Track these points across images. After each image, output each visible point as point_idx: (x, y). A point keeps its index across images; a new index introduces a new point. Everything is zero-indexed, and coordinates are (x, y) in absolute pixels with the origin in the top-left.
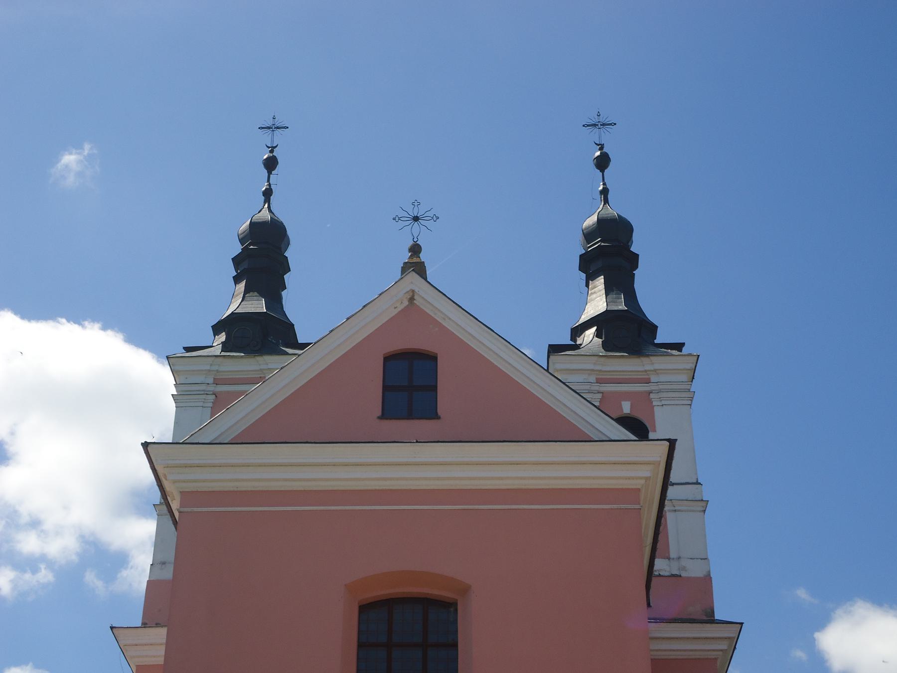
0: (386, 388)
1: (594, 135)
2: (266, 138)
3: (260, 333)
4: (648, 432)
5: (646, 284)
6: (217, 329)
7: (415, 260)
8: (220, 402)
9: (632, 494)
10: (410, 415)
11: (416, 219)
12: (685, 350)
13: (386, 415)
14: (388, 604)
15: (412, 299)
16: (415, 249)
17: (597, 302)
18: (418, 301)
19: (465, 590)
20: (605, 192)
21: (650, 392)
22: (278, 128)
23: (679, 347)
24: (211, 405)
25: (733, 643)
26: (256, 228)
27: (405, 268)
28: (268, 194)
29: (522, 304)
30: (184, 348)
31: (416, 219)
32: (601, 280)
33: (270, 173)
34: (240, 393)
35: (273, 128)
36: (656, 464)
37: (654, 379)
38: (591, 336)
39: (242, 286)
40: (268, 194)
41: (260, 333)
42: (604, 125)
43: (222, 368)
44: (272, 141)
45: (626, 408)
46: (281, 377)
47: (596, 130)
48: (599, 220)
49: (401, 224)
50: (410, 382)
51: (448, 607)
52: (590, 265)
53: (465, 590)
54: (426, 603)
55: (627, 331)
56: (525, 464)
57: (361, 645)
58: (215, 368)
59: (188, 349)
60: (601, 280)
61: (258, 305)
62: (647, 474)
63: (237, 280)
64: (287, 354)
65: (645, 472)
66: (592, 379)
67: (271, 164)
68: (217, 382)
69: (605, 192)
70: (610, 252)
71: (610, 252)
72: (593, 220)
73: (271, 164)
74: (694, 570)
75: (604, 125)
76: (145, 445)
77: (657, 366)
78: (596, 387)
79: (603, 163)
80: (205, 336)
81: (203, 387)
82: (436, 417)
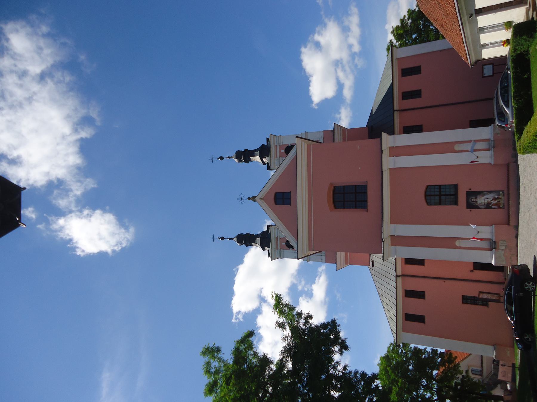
0: (283, 204)
1: (215, 160)
2: (216, 240)
3: (265, 240)
5: (251, 148)
6: (264, 250)
9: (308, 146)
13: (290, 204)
16: (249, 199)
17: (257, 158)
19: (331, 184)
20: (229, 157)
23: (268, 139)
27: (254, 201)
28: (230, 239)
29: (261, 176)
32: (251, 158)
40: (230, 239)
45: (283, 151)
50: (282, 199)
51: (335, 188)
53: (331, 184)
54: (334, 193)
56: (490, 28)
59: (269, 256)
60: (251, 158)
61: (258, 239)
67: (222, 238)
68: (277, 249)
69: (229, 157)
70: (245, 156)
71: (245, 156)
72: (236, 160)
73: (222, 238)
74: (322, 134)
79: (222, 158)
80: (266, 252)
82: (290, 192)
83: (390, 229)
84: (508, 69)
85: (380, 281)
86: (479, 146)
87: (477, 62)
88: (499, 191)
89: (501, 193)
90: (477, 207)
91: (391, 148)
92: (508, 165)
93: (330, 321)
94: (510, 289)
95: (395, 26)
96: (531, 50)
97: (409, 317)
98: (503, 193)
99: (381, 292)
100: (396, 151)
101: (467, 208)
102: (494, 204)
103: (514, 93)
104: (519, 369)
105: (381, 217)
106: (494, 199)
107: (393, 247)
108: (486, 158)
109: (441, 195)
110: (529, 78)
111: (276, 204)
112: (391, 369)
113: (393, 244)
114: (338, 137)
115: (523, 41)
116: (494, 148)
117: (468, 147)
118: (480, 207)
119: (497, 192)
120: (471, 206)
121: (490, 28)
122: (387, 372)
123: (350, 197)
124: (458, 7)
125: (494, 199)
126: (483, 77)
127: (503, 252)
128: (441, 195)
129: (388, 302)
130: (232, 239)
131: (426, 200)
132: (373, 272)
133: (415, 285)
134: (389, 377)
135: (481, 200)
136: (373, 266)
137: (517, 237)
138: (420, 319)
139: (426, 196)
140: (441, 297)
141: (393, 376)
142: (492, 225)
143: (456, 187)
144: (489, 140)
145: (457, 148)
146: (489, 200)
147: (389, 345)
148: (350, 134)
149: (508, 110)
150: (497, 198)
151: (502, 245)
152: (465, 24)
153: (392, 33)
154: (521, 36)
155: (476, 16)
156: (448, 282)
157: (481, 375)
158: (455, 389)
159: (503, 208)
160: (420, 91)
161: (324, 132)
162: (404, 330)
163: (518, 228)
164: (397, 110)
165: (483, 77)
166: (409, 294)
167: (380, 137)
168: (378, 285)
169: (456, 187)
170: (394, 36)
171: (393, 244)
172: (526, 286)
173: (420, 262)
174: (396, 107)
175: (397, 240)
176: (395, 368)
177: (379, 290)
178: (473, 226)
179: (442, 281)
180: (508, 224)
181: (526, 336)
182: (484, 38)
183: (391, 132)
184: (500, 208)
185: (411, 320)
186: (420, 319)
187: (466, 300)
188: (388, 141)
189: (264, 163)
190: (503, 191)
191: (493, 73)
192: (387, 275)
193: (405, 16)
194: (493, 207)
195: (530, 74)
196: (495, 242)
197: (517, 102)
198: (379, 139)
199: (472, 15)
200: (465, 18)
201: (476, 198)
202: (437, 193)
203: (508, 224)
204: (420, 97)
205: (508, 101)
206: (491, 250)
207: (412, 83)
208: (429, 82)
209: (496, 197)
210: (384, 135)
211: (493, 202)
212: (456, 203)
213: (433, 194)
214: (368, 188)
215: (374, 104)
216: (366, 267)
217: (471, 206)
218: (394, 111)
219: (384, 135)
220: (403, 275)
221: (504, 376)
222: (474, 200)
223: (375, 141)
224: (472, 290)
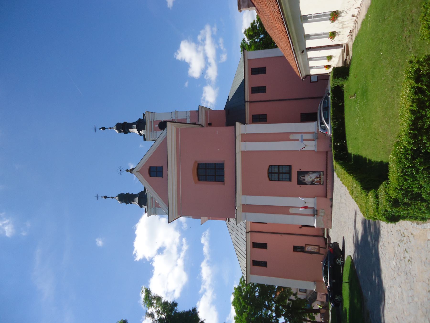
3: (143, 198)
6: (141, 207)
8: (157, 206)
10: (162, 172)
11: (121, 170)
12: (144, 113)
14: (198, 175)
16: (127, 171)
17: (135, 131)
18: (138, 170)
19: (196, 161)
20: (110, 128)
23: (144, 115)
26: (120, 200)
28: (112, 198)
29: (138, 148)
31: (121, 170)
34: (155, 202)
36: (171, 124)
37: (151, 120)
39: (132, 202)
40: (112, 198)
45: (157, 126)
46: (151, 193)
48: (117, 130)
50: (155, 172)
52: (126, 131)
53: (196, 161)
54: (198, 168)
55: (141, 124)
56: (315, 17)
57: (206, 181)
59: (146, 212)
61: (137, 199)
63: (131, 203)
65: (173, 127)
66: (152, 208)
67: (106, 197)
68: (153, 207)
69: (110, 128)
71: (124, 127)
73: (106, 197)
74: (189, 114)
76: (169, 223)
78: (153, 131)
79: (104, 128)
82: (162, 167)
83: (241, 199)
84: (329, 94)
85: (235, 238)
86: (306, 137)
87: (306, 76)
88: (320, 172)
89: (321, 173)
90: (305, 184)
91: (242, 135)
92: (327, 152)
93: (191, 310)
94: (327, 264)
95: (247, 28)
96: (345, 85)
97: (256, 263)
98: (323, 173)
99: (234, 242)
100: (247, 138)
101: (298, 184)
102: (317, 182)
103: (335, 155)
104: (331, 311)
105: (235, 176)
106: (317, 178)
107: (244, 213)
108: (311, 146)
109: (279, 173)
110: (343, 105)
111: (150, 176)
112: (242, 298)
113: (243, 211)
115: (339, 81)
116: (317, 139)
117: (298, 137)
118: (307, 183)
119: (319, 172)
120: (301, 182)
121: (315, 17)
122: (239, 300)
123: (210, 172)
124: (294, 48)
125: (317, 178)
126: (311, 82)
127: (322, 218)
128: (279, 173)
129: (240, 251)
130: (114, 198)
131: (268, 176)
132: (229, 226)
133: (260, 239)
134: (241, 304)
135: (308, 178)
136: (229, 221)
137: (332, 206)
138: (264, 264)
139: (269, 173)
140: (280, 247)
141: (243, 304)
142: (314, 197)
143: (290, 167)
144: (314, 132)
145: (291, 137)
146: (313, 178)
147: (241, 278)
149: (328, 126)
150: (319, 177)
151: (321, 213)
152: (298, 56)
153: (244, 33)
154: (338, 78)
155: (307, 51)
156: (283, 235)
157: (306, 292)
158: (287, 307)
159: (323, 185)
160: (265, 68)
161: (191, 112)
162: (252, 273)
163: (332, 200)
164: (248, 102)
165: (311, 82)
166: (256, 245)
167: (234, 125)
168: (232, 236)
169: (290, 167)
170: (246, 35)
171: (243, 211)
172: (338, 261)
174: (247, 99)
175: (247, 208)
176: (245, 298)
177: (233, 240)
178: (302, 199)
179: (279, 235)
180: (326, 196)
181: (336, 297)
182: (311, 64)
184: (320, 184)
185: (257, 264)
186: (264, 264)
187: (296, 249)
188: (240, 128)
189: (141, 135)
190: (323, 172)
191: (318, 80)
192: (239, 230)
193: (254, 21)
194: (316, 183)
195: (344, 103)
196: (317, 210)
197: (334, 123)
198: (233, 127)
199: (304, 51)
200: (299, 53)
201: (304, 177)
202: (277, 171)
203: (326, 196)
204: (265, 73)
205: (328, 119)
206: (314, 216)
207: (259, 80)
208: (272, 84)
209: (318, 176)
210: (237, 124)
211: (316, 180)
212: (290, 180)
213: (274, 172)
214: (225, 166)
215: (231, 92)
216: (224, 221)
217: (301, 182)
218: (245, 102)
219: (237, 124)
220: (251, 231)
221: (321, 298)
222: (303, 178)
223: (231, 128)
224: (300, 242)
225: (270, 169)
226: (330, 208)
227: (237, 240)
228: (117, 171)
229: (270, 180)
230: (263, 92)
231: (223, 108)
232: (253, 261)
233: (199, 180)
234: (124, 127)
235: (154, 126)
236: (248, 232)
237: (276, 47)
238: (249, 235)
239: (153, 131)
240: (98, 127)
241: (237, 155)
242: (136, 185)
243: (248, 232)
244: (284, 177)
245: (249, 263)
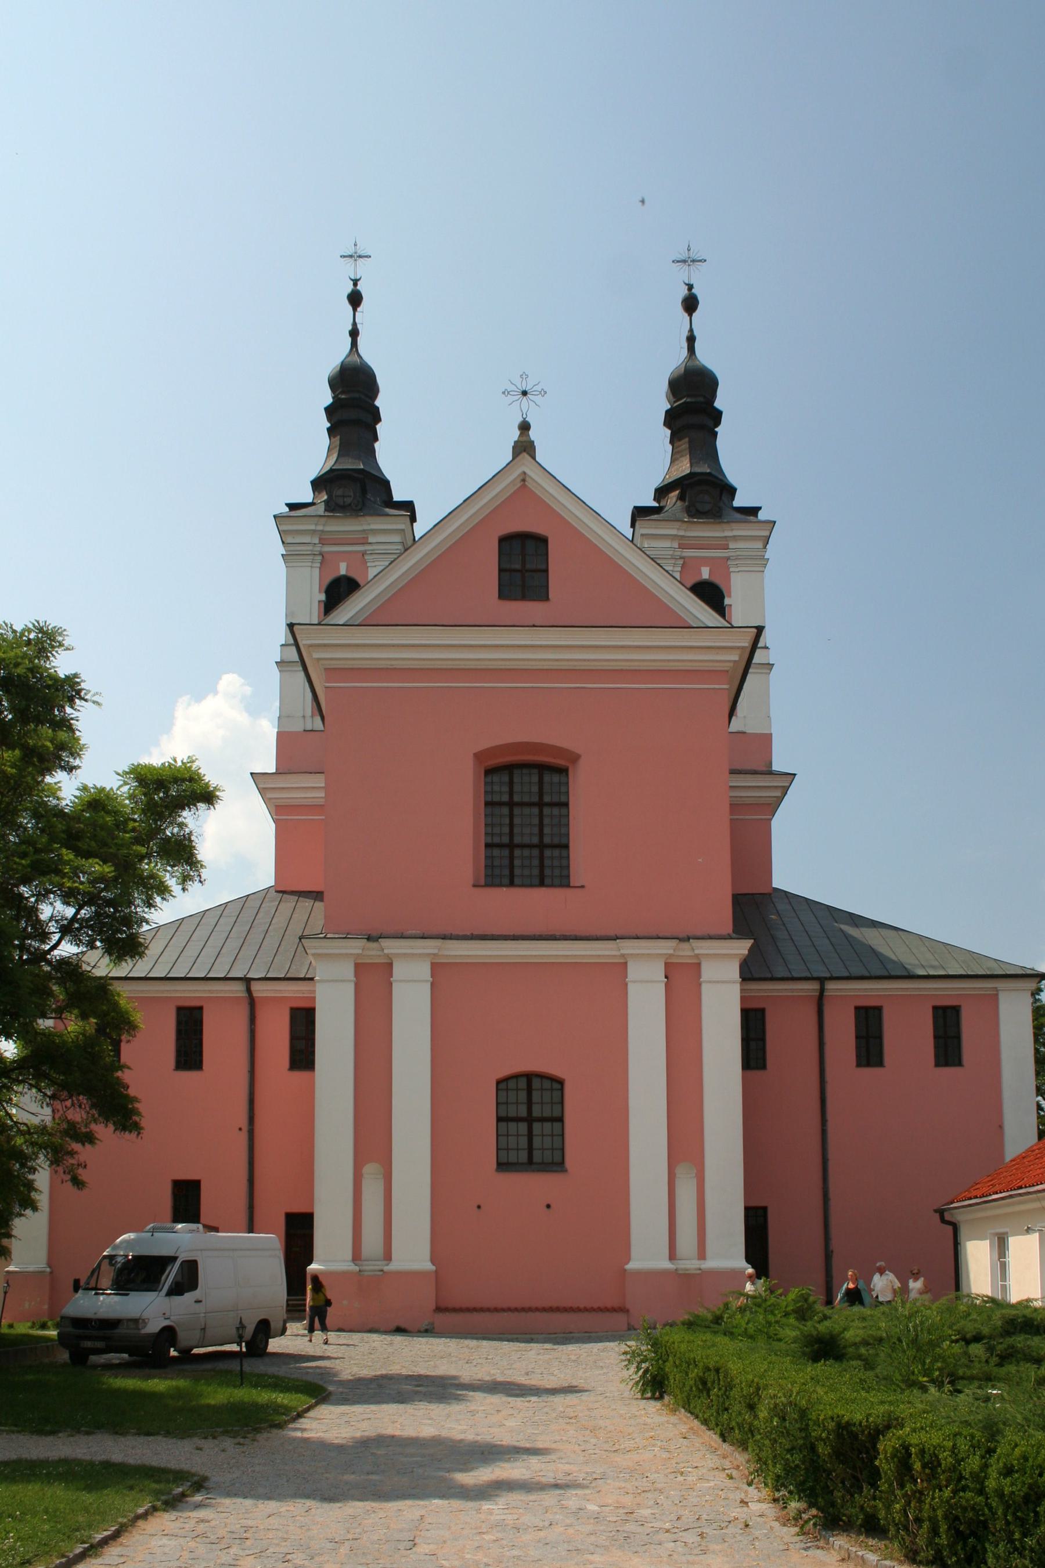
3: (353, 486)
4: (724, 597)
7: (524, 439)
11: (524, 393)
12: (762, 516)
15: (524, 480)
16: (525, 427)
18: (529, 484)
19: (575, 758)
21: (728, 558)
22: (360, 257)
23: (754, 511)
24: (318, 565)
25: (785, 790)
30: (287, 505)
31: (524, 393)
33: (355, 310)
35: (355, 257)
38: (674, 500)
41: (353, 486)
42: (693, 261)
43: (328, 529)
44: (355, 273)
45: (705, 574)
47: (686, 267)
49: (510, 398)
53: (575, 758)
54: (542, 768)
58: (320, 528)
62: (736, 658)
64: (388, 515)
65: (735, 657)
71: (693, 406)
75: (693, 261)
77: (373, 527)
80: (306, 495)
81: (310, 548)
100: (682, 985)
108: (647, 1253)
109: (530, 1121)
114: (751, 787)
123: (525, 817)
128: (530, 1121)
131: (516, 1077)
133: (222, 1038)
137: (400, 1330)
142: (49, 1265)
148: (750, 844)
156: (244, 1136)
164: (822, 990)
166: (190, 1024)
173: (303, 1055)
179: (244, 1123)
180: (439, 1309)
183: (749, 972)
203: (439, 1309)
207: (908, 1037)
210: (742, 947)
219: (742, 947)
220: (252, 1001)
223: (724, 916)
225: (547, 1084)
226: (393, 1326)
227: (216, 941)
228: (524, 376)
229: (498, 1082)
230: (858, 1056)
231: (779, 881)
232: (200, 1009)
233: (488, 772)
234: (693, 406)
235: (705, 561)
236: (249, 990)
237: (136, 1128)
238: (237, 990)
239: (318, 549)
240: (363, 269)
241: (610, 944)
242: (435, 466)
243: (249, 990)
244: (512, 1140)
245: (190, 993)
